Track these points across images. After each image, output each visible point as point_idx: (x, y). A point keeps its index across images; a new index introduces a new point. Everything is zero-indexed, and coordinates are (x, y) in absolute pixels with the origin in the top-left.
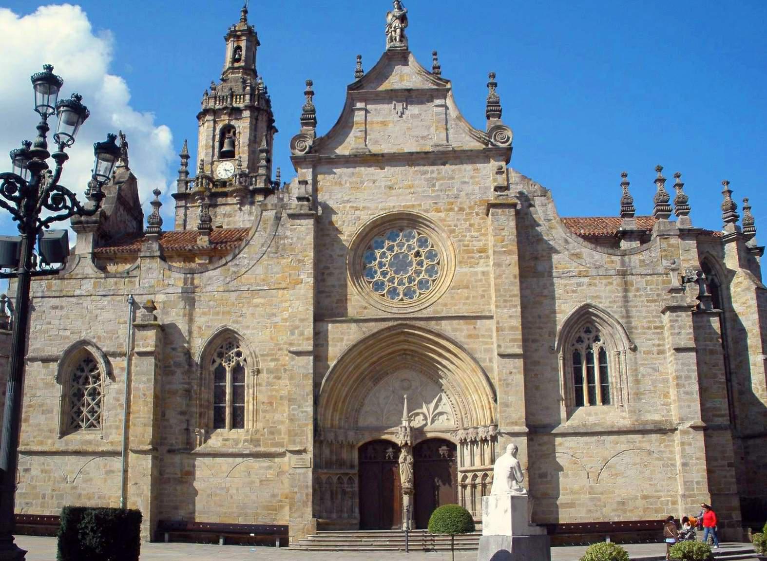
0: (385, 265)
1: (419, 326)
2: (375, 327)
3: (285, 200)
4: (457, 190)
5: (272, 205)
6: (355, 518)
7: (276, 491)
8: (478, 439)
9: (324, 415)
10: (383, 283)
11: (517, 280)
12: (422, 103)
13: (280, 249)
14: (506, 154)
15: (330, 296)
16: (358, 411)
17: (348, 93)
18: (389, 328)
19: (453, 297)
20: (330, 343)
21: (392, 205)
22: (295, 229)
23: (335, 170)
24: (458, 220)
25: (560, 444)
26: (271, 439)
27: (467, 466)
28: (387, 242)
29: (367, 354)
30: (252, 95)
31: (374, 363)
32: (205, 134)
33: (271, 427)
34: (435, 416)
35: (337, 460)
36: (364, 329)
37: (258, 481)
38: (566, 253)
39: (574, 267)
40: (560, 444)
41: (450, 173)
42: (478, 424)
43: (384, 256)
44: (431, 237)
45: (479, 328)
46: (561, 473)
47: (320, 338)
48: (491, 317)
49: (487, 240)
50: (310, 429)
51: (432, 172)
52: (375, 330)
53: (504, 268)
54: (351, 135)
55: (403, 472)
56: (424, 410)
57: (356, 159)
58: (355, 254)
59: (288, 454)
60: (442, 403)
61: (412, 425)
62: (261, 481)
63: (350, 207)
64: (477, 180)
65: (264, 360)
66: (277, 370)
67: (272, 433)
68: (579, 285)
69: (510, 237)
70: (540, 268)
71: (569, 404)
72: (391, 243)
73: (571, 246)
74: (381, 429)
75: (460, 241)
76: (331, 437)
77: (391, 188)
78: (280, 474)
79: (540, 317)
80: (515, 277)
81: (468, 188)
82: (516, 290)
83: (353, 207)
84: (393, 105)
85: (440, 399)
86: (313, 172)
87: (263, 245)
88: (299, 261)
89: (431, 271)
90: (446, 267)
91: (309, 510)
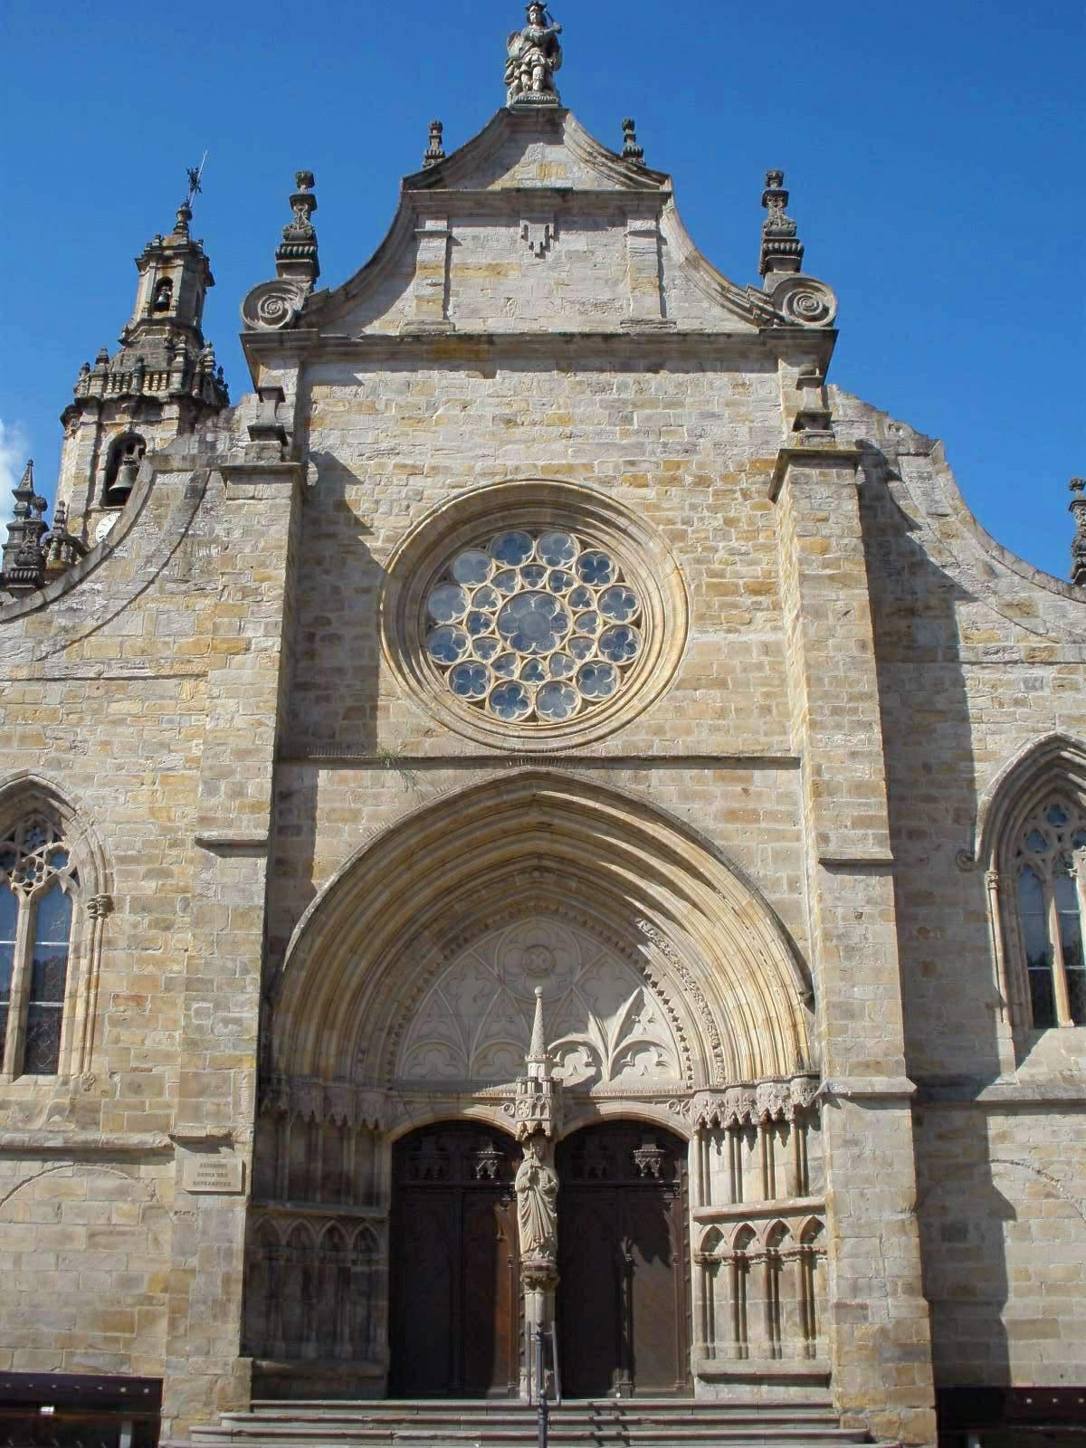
0: (487, 625)
1: (584, 779)
2: (450, 782)
3: (221, 447)
4: (691, 433)
5: (184, 458)
6: (376, 1361)
7: (136, 1267)
8: (754, 1120)
9: (294, 1037)
10: (480, 673)
11: (870, 655)
12: (596, 227)
13: (195, 572)
14: (817, 350)
15: (327, 699)
16: (396, 1032)
17: (404, 195)
18: (495, 785)
19: (679, 710)
20: (321, 824)
21: (511, 463)
22: (240, 507)
23: (360, 376)
24: (693, 507)
25: (1003, 1136)
26: (129, 1107)
27: (720, 1201)
28: (494, 563)
29: (428, 861)
30: (187, 373)
31: (448, 891)
32: (78, 453)
33: (135, 1069)
34: (623, 1054)
35: (326, 1176)
36: (422, 788)
37: (82, 1231)
38: (992, 600)
39: (1016, 639)
40: (1003, 1136)
41: (672, 391)
42: (754, 1075)
43: (480, 594)
44: (618, 554)
45: (759, 795)
46: (1007, 1226)
47: (291, 812)
48: (794, 763)
49: (775, 563)
50: (249, 1068)
51: (623, 387)
52: (457, 790)
53: (831, 620)
54: (410, 291)
55: (526, 1216)
56: (593, 1035)
57: (416, 347)
58: (405, 587)
59: (180, 1151)
60: (644, 1017)
61: (556, 1073)
62: (92, 1235)
63: (396, 466)
64: (743, 410)
65: (127, 875)
66: (165, 904)
67: (136, 1088)
68: (1032, 685)
69: (846, 541)
70: (923, 637)
71: (1017, 1020)
72: (506, 567)
73: (1002, 584)
74: (465, 1089)
75: (698, 561)
76: (310, 1102)
77: (509, 422)
78: (151, 1212)
79: (927, 768)
80: (863, 646)
81: (718, 431)
82: (868, 681)
83: (405, 466)
84: (520, 231)
85: (638, 1006)
86: (301, 378)
87: (149, 560)
88: (245, 592)
89: (618, 642)
90: (659, 632)
91: (231, 1329)
